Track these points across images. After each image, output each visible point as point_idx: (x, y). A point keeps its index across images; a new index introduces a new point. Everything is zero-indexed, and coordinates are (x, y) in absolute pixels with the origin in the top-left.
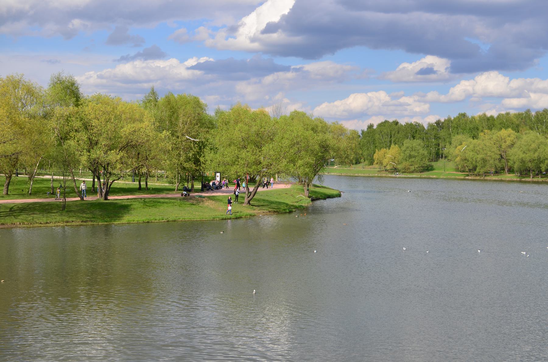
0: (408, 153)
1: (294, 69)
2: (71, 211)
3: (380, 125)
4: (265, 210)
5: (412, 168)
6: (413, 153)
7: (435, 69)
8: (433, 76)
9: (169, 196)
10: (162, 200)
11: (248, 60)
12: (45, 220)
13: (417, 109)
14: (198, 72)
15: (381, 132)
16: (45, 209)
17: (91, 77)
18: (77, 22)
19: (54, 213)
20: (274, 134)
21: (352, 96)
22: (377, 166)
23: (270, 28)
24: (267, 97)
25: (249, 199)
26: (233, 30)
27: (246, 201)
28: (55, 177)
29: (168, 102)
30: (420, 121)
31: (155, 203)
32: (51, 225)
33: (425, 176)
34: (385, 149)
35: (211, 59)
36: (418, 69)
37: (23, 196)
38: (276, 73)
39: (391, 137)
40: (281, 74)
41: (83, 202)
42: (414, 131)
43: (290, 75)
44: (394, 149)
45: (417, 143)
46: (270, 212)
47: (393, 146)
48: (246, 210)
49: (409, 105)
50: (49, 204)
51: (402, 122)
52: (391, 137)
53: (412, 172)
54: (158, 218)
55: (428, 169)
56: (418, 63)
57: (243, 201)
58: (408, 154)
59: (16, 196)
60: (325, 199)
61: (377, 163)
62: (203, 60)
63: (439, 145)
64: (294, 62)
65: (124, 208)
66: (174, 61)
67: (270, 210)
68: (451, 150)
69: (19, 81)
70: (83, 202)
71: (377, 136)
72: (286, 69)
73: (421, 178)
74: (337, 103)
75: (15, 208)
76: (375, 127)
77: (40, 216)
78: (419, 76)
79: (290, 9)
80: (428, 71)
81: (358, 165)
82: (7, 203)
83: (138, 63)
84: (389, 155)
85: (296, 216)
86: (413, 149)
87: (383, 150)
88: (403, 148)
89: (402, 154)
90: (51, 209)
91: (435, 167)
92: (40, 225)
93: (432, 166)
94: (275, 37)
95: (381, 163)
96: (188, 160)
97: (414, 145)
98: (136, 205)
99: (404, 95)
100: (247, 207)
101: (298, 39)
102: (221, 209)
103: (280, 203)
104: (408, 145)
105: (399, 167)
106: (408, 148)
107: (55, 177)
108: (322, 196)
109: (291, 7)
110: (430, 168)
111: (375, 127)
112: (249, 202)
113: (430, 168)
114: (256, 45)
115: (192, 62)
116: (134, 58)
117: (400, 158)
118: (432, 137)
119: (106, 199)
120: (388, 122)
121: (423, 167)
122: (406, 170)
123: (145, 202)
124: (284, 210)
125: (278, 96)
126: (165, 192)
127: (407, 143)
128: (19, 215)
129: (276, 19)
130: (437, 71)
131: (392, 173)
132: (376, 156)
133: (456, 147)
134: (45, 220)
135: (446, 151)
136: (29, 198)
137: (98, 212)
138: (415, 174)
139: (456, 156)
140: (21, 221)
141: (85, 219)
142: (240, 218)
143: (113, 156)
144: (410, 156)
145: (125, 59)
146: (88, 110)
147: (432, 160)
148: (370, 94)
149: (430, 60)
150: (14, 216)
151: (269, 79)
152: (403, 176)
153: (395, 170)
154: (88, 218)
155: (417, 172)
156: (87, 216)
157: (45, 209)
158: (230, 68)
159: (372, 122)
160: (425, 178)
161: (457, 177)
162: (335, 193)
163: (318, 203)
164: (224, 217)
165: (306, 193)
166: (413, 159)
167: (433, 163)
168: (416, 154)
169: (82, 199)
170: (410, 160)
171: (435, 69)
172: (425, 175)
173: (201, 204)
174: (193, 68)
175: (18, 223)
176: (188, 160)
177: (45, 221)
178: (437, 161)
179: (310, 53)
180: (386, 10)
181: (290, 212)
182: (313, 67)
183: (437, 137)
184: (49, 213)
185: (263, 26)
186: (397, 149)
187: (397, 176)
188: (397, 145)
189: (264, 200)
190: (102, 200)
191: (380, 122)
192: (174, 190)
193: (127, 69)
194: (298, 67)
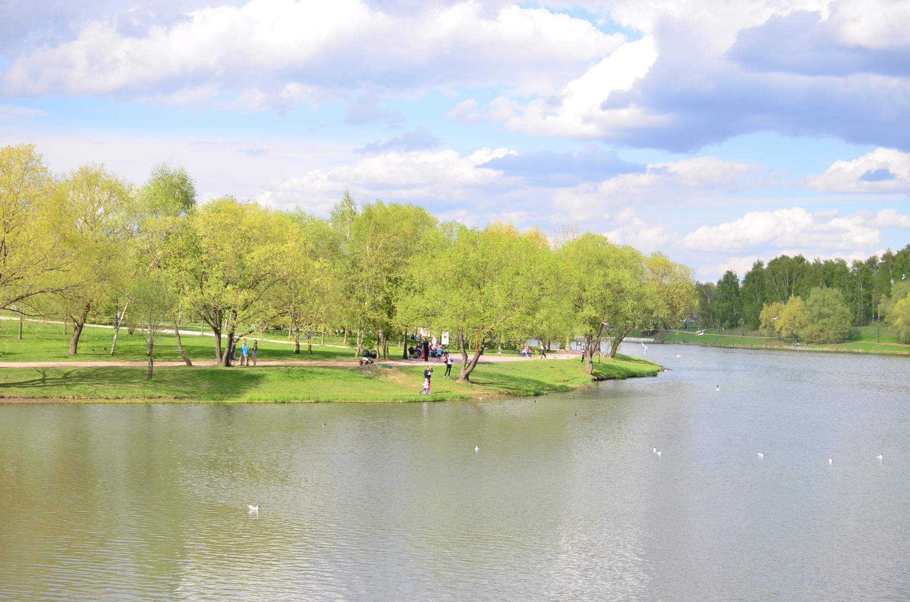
0: (816, 310)
1: (652, 169)
2: (161, 382)
3: (773, 263)
4: (492, 390)
5: (824, 337)
6: (825, 310)
7: (892, 171)
8: (886, 184)
9: (339, 364)
10: (321, 370)
11: (576, 154)
12: (114, 393)
13: (860, 239)
14: (492, 173)
15: (774, 275)
16: (120, 377)
17: (318, 178)
18: (293, 89)
19: (134, 383)
20: (500, 265)
21: (749, 217)
22: (765, 331)
23: (615, 102)
24: (606, 216)
25: (467, 371)
26: (554, 103)
27: (462, 374)
28: (205, 334)
29: (369, 215)
30: (842, 257)
31: (304, 373)
32: (125, 401)
33: (845, 349)
34: (778, 303)
35: (512, 152)
36: (862, 171)
37: (99, 356)
38: (621, 176)
39: (790, 283)
40: (630, 178)
41: (190, 368)
42: (831, 274)
43: (644, 179)
44: (794, 304)
45: (832, 295)
46: (500, 393)
47: (792, 298)
48: (460, 389)
49: (847, 231)
50: (131, 370)
51: (810, 259)
52: (790, 283)
53: (824, 342)
54: (300, 397)
55: (850, 337)
56: (862, 160)
57: (458, 375)
58: (816, 312)
59: (88, 357)
60: (624, 378)
61: (765, 327)
62: (500, 153)
63: (870, 298)
64: (653, 158)
65: (254, 379)
66: (449, 154)
67: (502, 390)
68: (888, 309)
69: (97, 175)
70: (190, 368)
71: (767, 281)
72: (640, 169)
73: (836, 352)
74: (724, 227)
75: (73, 374)
76: (765, 266)
77: (111, 387)
78: (866, 183)
79: (650, 69)
80: (881, 174)
81: (735, 330)
82: (61, 366)
83: (394, 157)
84: (783, 313)
85: (542, 403)
86: (824, 303)
87: (776, 305)
88: (809, 302)
89: (807, 312)
90: (131, 378)
91: (863, 334)
92: (107, 401)
93: (858, 333)
94: (628, 115)
95: (772, 326)
96: (375, 306)
97: (827, 296)
98: (273, 375)
99: (837, 216)
100: (462, 385)
101: (660, 120)
102: (414, 386)
103: (528, 381)
104: (817, 296)
105: (801, 333)
106: (816, 301)
107: (199, 333)
108: (619, 373)
109: (651, 65)
110: (855, 336)
111: (765, 266)
112: (467, 377)
113: (855, 336)
114: (591, 129)
115: (483, 156)
116: (388, 147)
117: (803, 318)
118: (860, 283)
119: (228, 365)
120: (788, 258)
121: (841, 334)
122: (812, 340)
123: (288, 372)
124: (527, 391)
125: (625, 214)
126: (339, 358)
127: (816, 293)
128: (75, 385)
129: (625, 85)
130: (894, 174)
131: (790, 343)
132: (763, 315)
133: (896, 302)
134: (114, 393)
135: (880, 308)
136: (165, 367)
137: (206, 385)
138: (828, 345)
139: (897, 317)
140: (75, 393)
141: (180, 395)
142: (442, 400)
143: (233, 297)
144: (821, 316)
145: (374, 149)
146: (199, 225)
147: (859, 324)
148: (778, 213)
149: (882, 156)
150: (67, 385)
151: (610, 185)
152: (808, 349)
153: (795, 338)
154: (187, 393)
155: (831, 342)
156: (187, 390)
157: (120, 377)
158: (544, 168)
159: (761, 259)
160: (843, 353)
161: (898, 352)
162: (648, 368)
163: (602, 384)
164: (413, 398)
165: (588, 367)
166: (825, 320)
167: (860, 328)
168: (831, 312)
169: (189, 364)
170: (820, 322)
171: (892, 170)
172: (844, 347)
173: (382, 378)
174: (485, 166)
175: (71, 397)
176: (375, 306)
177: (114, 395)
178: (867, 325)
179: (679, 141)
180: (811, 71)
181: (537, 395)
182: (686, 166)
183: (867, 285)
184: (126, 382)
185: (604, 97)
186: (799, 304)
187: (798, 348)
188: (799, 297)
189: (501, 376)
190: (222, 366)
191: (773, 258)
192: (353, 355)
193: (377, 166)
194: (659, 165)
